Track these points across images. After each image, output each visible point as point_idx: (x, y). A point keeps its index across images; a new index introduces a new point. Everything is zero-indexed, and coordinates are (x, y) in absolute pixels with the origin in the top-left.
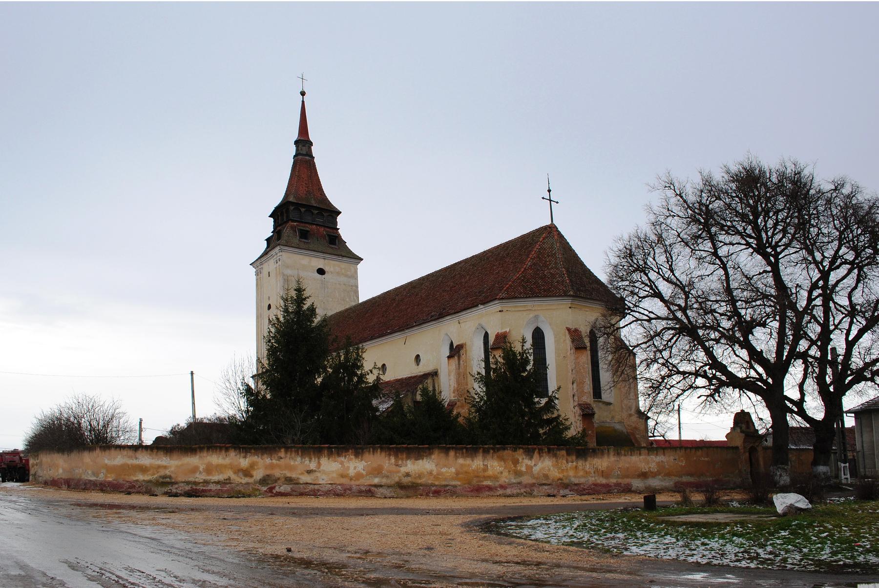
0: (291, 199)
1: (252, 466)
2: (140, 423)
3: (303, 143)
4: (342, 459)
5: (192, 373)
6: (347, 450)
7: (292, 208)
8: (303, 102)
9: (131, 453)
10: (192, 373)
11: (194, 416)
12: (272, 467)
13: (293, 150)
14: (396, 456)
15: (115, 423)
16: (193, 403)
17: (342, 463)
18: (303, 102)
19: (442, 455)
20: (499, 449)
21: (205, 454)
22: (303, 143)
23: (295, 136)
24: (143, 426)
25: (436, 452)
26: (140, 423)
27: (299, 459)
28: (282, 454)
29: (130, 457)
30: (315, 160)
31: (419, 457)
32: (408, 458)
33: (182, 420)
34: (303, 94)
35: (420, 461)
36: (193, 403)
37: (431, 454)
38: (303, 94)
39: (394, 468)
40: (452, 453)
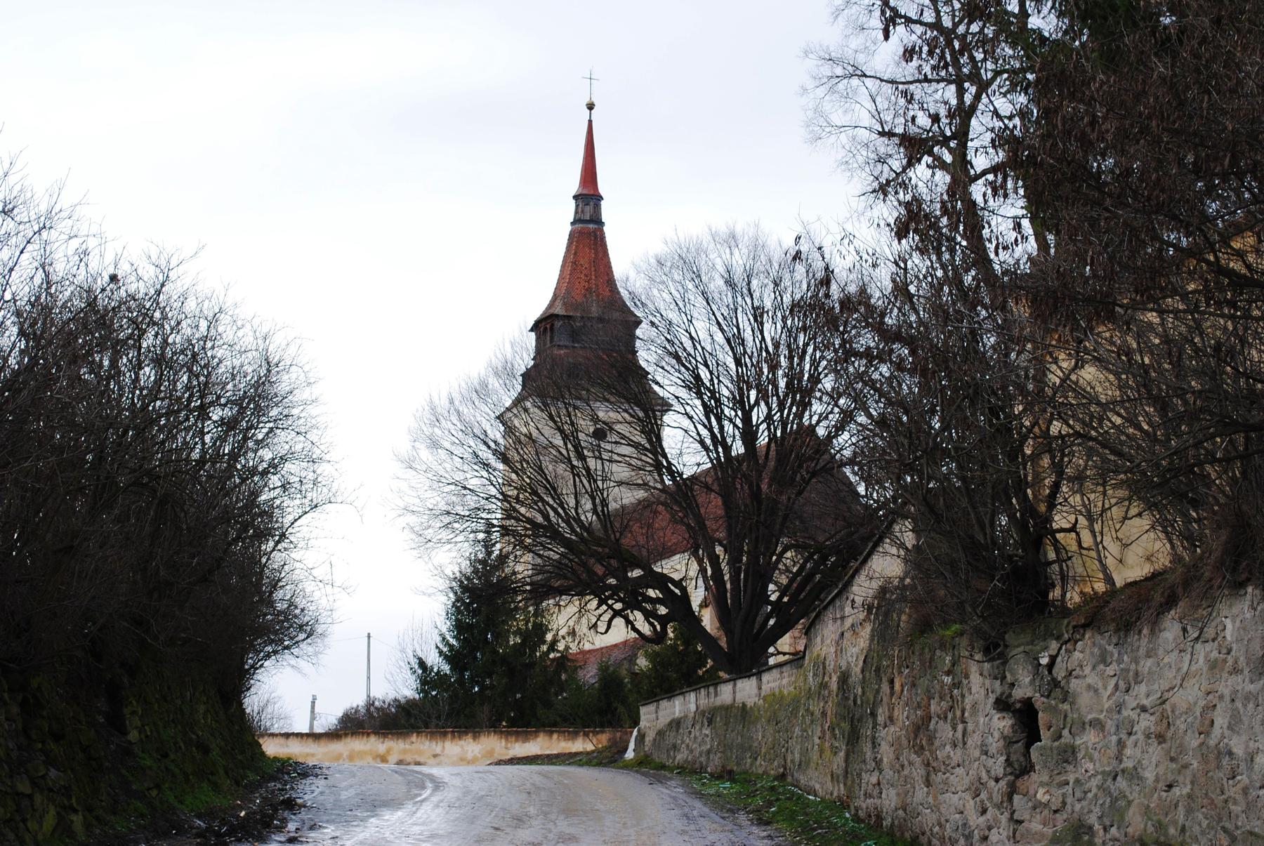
0: (558, 310)
1: (388, 751)
2: (313, 703)
3: (588, 199)
4: (462, 742)
5: (369, 637)
6: (466, 733)
7: (558, 324)
8: (590, 122)
9: (282, 740)
10: (369, 637)
11: (369, 696)
12: (405, 751)
13: (568, 210)
14: (507, 739)
15: (269, 709)
16: (369, 678)
17: (462, 747)
18: (590, 122)
19: (547, 738)
20: (598, 733)
21: (349, 740)
22: (588, 199)
23: (573, 184)
24: (316, 710)
25: (542, 735)
26: (313, 703)
27: (427, 743)
28: (414, 738)
29: (282, 745)
30: (605, 228)
31: (526, 740)
32: (516, 741)
33: (359, 701)
34: (591, 107)
35: (527, 744)
36: (369, 678)
37: (536, 737)
38: (591, 107)
39: (504, 751)
40: (555, 736)
